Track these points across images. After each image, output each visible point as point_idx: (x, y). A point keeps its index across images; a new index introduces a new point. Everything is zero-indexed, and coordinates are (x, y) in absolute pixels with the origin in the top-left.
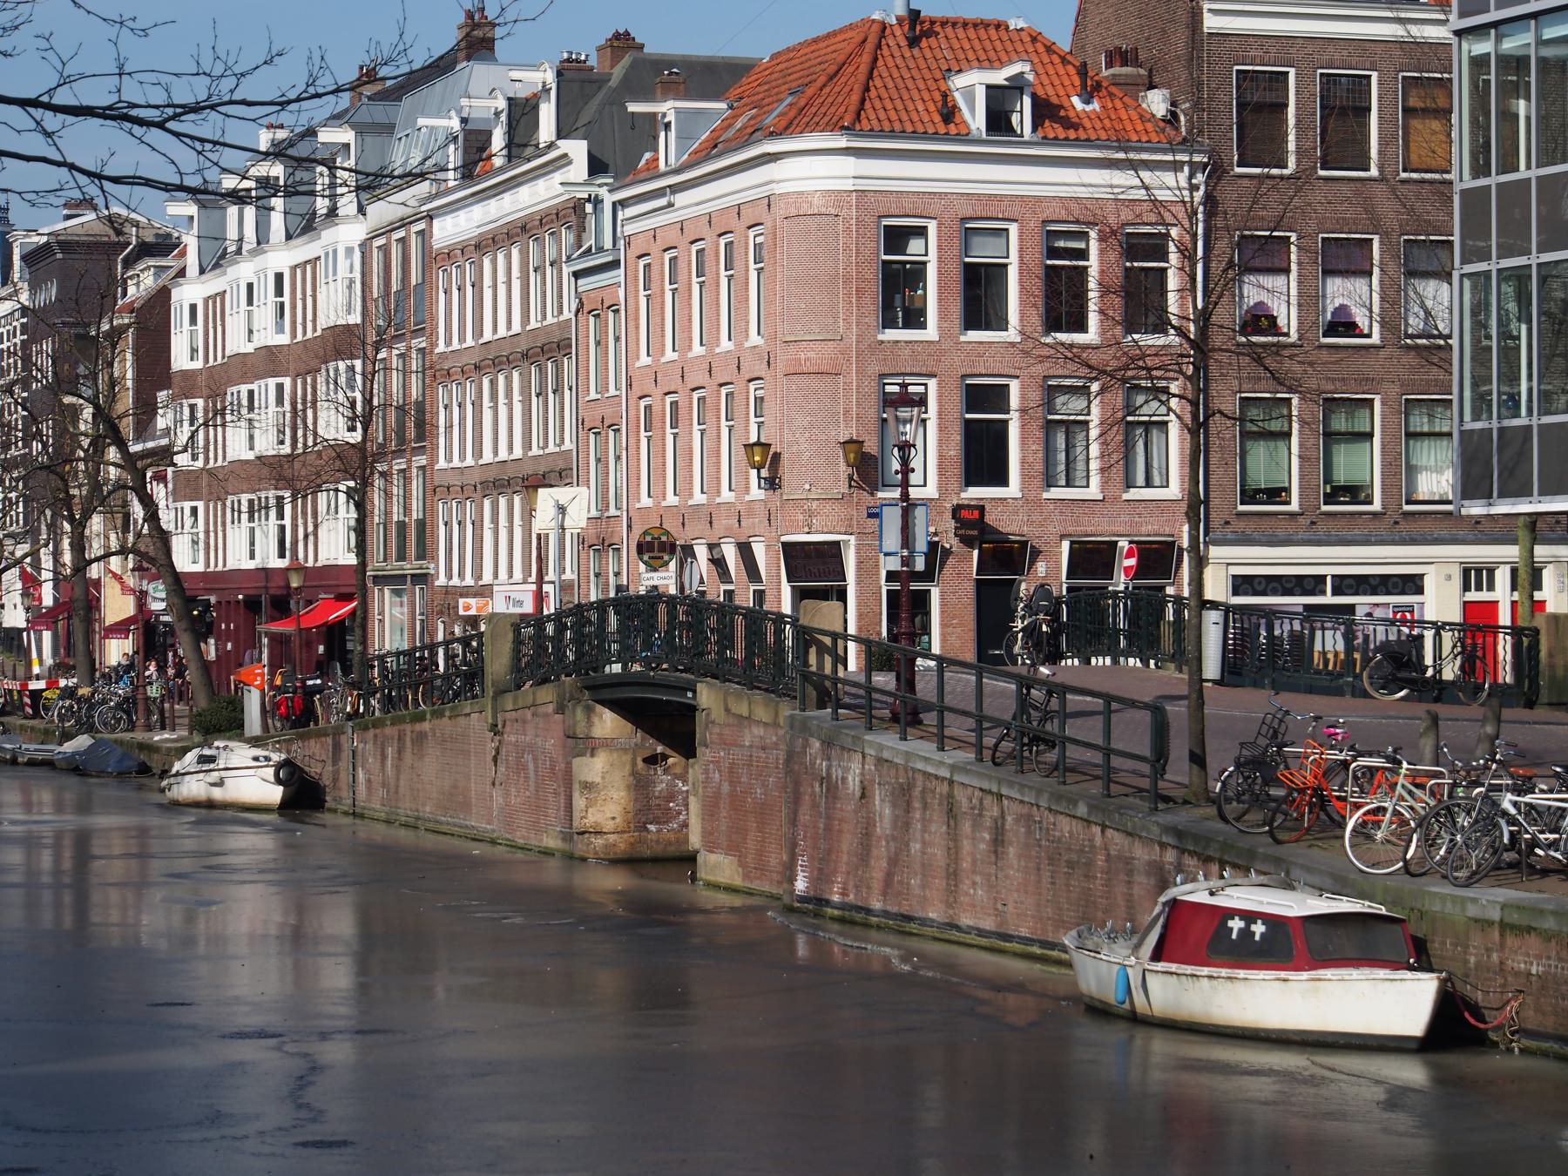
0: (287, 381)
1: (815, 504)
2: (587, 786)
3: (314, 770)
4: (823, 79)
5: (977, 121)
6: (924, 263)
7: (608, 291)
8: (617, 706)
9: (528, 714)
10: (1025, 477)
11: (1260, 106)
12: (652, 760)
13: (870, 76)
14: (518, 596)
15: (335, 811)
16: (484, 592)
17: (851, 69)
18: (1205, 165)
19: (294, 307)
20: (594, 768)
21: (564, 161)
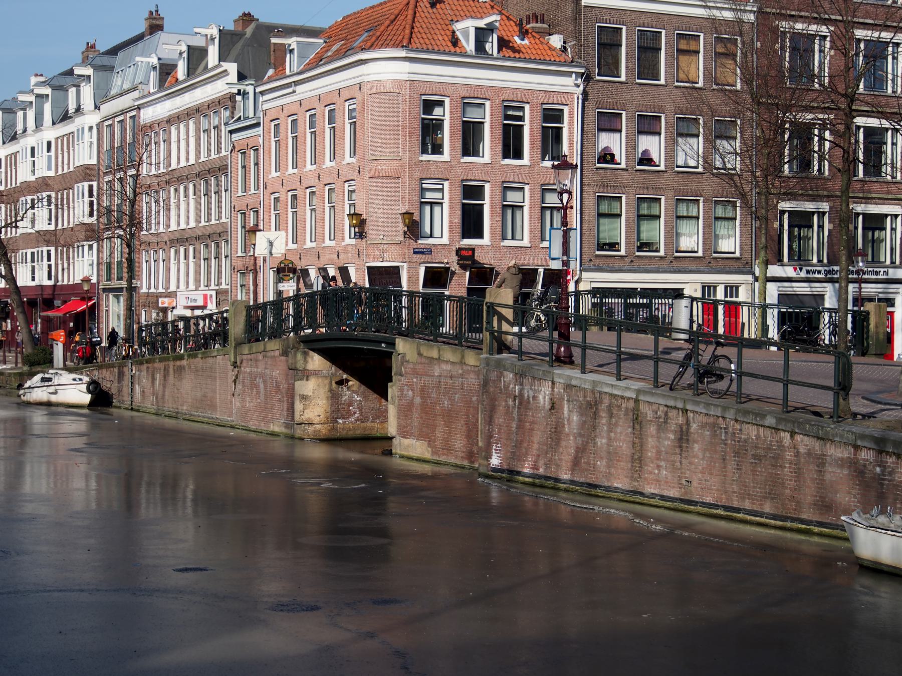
0: (53, 194)
1: (386, 246)
2: (304, 397)
3: (105, 385)
4: (388, 22)
5: (470, 46)
6: (443, 120)
7: (251, 139)
8: (323, 353)
9: (260, 357)
10: (492, 233)
11: (608, 44)
12: (340, 383)
13: (414, 22)
14: (193, 297)
15: (120, 408)
16: (173, 295)
17: (402, 18)
18: (583, 74)
19: (57, 158)
20: (308, 387)
21: (225, 73)
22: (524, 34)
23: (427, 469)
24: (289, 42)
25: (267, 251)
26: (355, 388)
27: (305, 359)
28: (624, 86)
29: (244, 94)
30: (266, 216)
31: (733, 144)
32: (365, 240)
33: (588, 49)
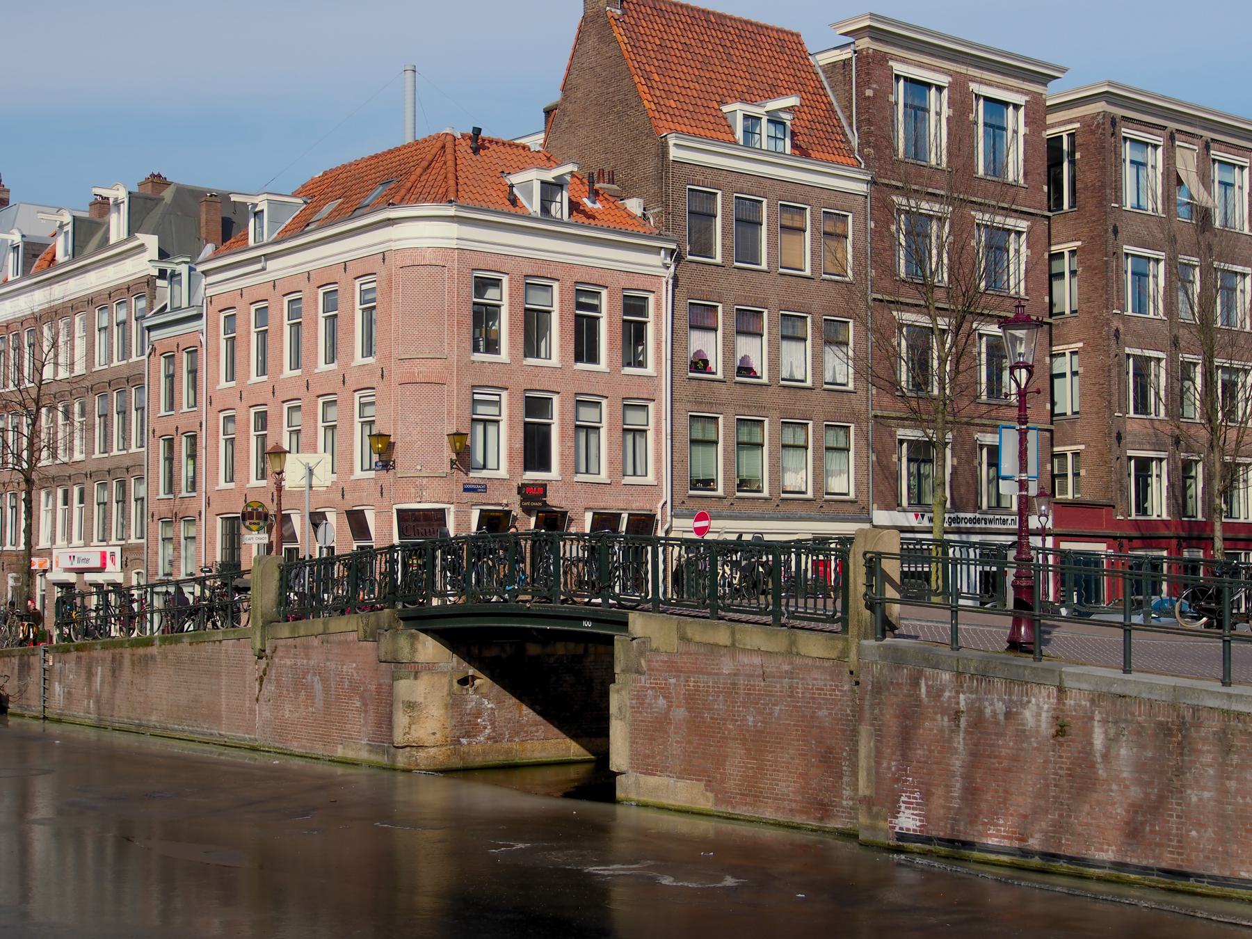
2: (411, 706)
4: (419, 171)
6: (499, 306)
9: (315, 642)
10: (563, 464)
12: (464, 681)
18: (673, 251)
21: (141, 248)
22: (595, 194)
23: (704, 827)
24: (255, 201)
25: (304, 482)
26: (484, 690)
27: (412, 645)
28: (720, 270)
29: (174, 276)
30: (211, 442)
31: (845, 349)
32: (391, 472)
33: (678, 219)
